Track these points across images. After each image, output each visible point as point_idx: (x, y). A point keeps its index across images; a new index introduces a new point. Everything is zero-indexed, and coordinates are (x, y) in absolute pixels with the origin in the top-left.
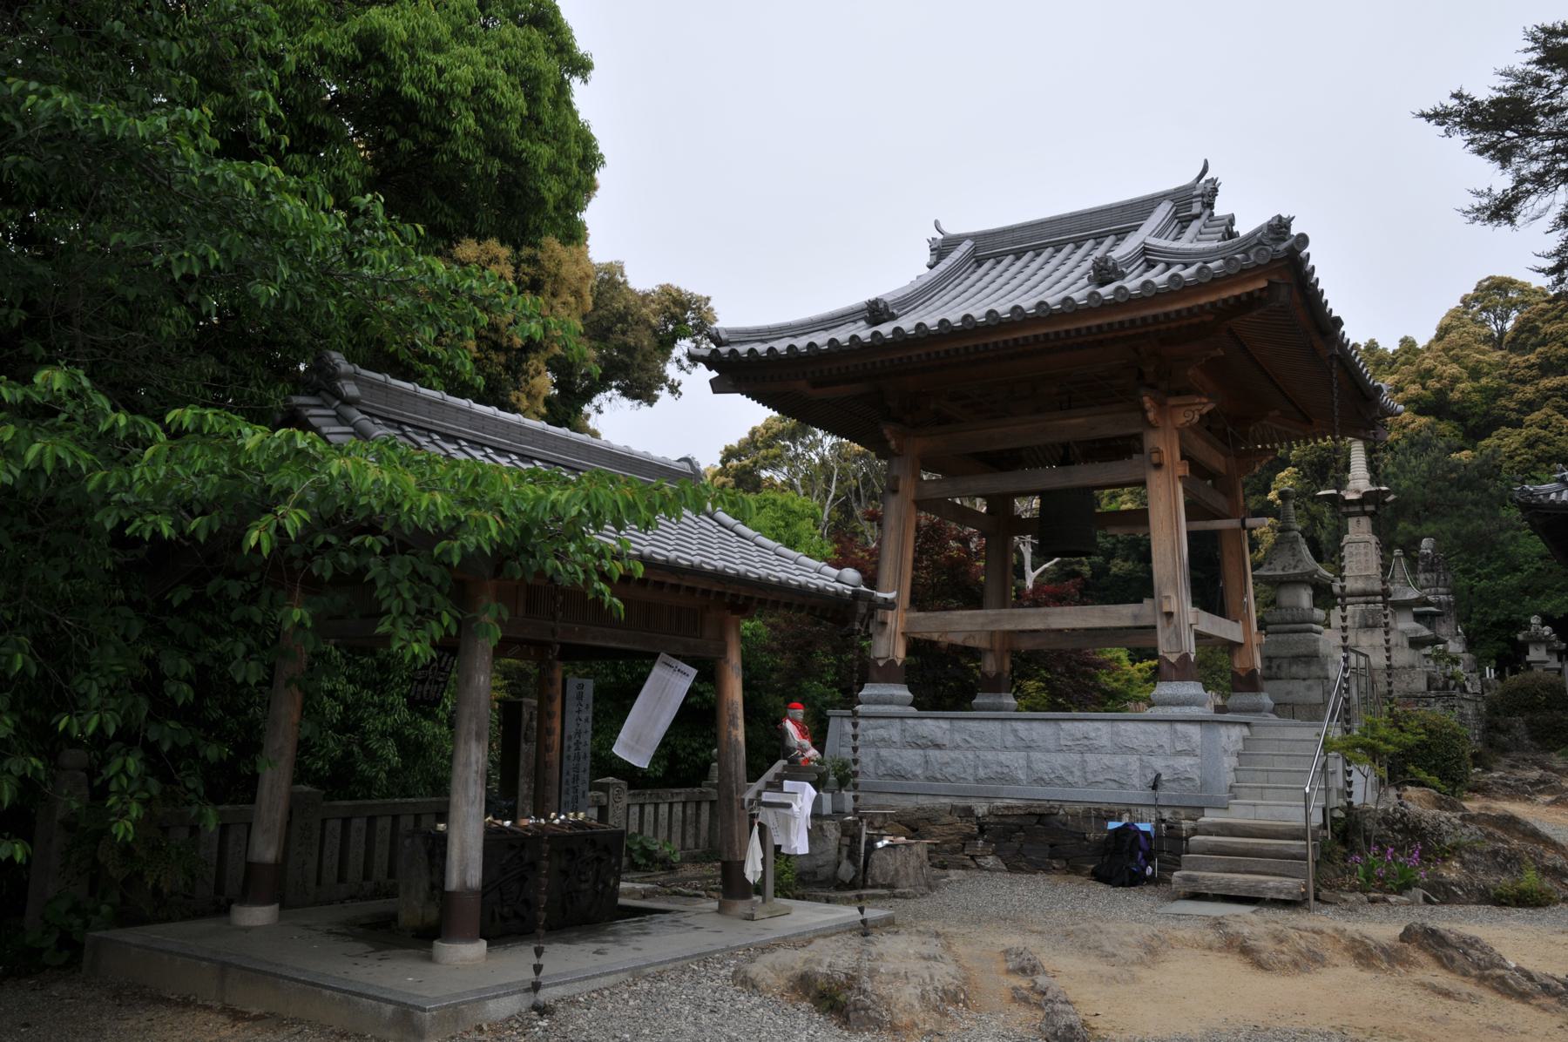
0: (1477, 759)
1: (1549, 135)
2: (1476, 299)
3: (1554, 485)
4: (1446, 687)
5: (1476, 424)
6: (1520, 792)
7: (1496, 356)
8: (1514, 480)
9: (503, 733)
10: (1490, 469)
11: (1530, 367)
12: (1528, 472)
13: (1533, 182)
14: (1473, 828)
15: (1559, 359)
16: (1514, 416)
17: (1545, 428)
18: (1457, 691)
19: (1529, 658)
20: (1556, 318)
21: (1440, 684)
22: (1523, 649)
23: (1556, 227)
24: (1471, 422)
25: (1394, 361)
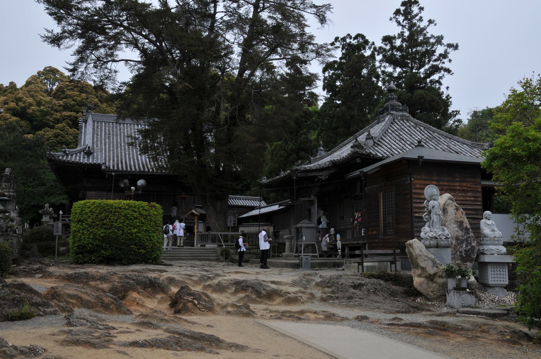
0: (15, 261)
1: (76, 18)
2: (43, 74)
3: (62, 153)
4: (7, 231)
5: (36, 123)
6: (30, 274)
7: (48, 99)
8: (47, 149)
9: (440, 95)
10: (39, 143)
11: (60, 106)
12: (53, 147)
13: (68, 34)
14: (6, 290)
15: (71, 105)
16: (52, 124)
17: (62, 131)
18: (11, 233)
19: (42, 220)
20: (72, 89)
21: (4, 230)
22: (41, 216)
23: (75, 54)
24: (35, 123)
25: (6, 91)
